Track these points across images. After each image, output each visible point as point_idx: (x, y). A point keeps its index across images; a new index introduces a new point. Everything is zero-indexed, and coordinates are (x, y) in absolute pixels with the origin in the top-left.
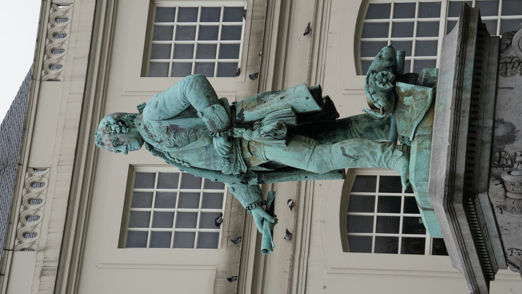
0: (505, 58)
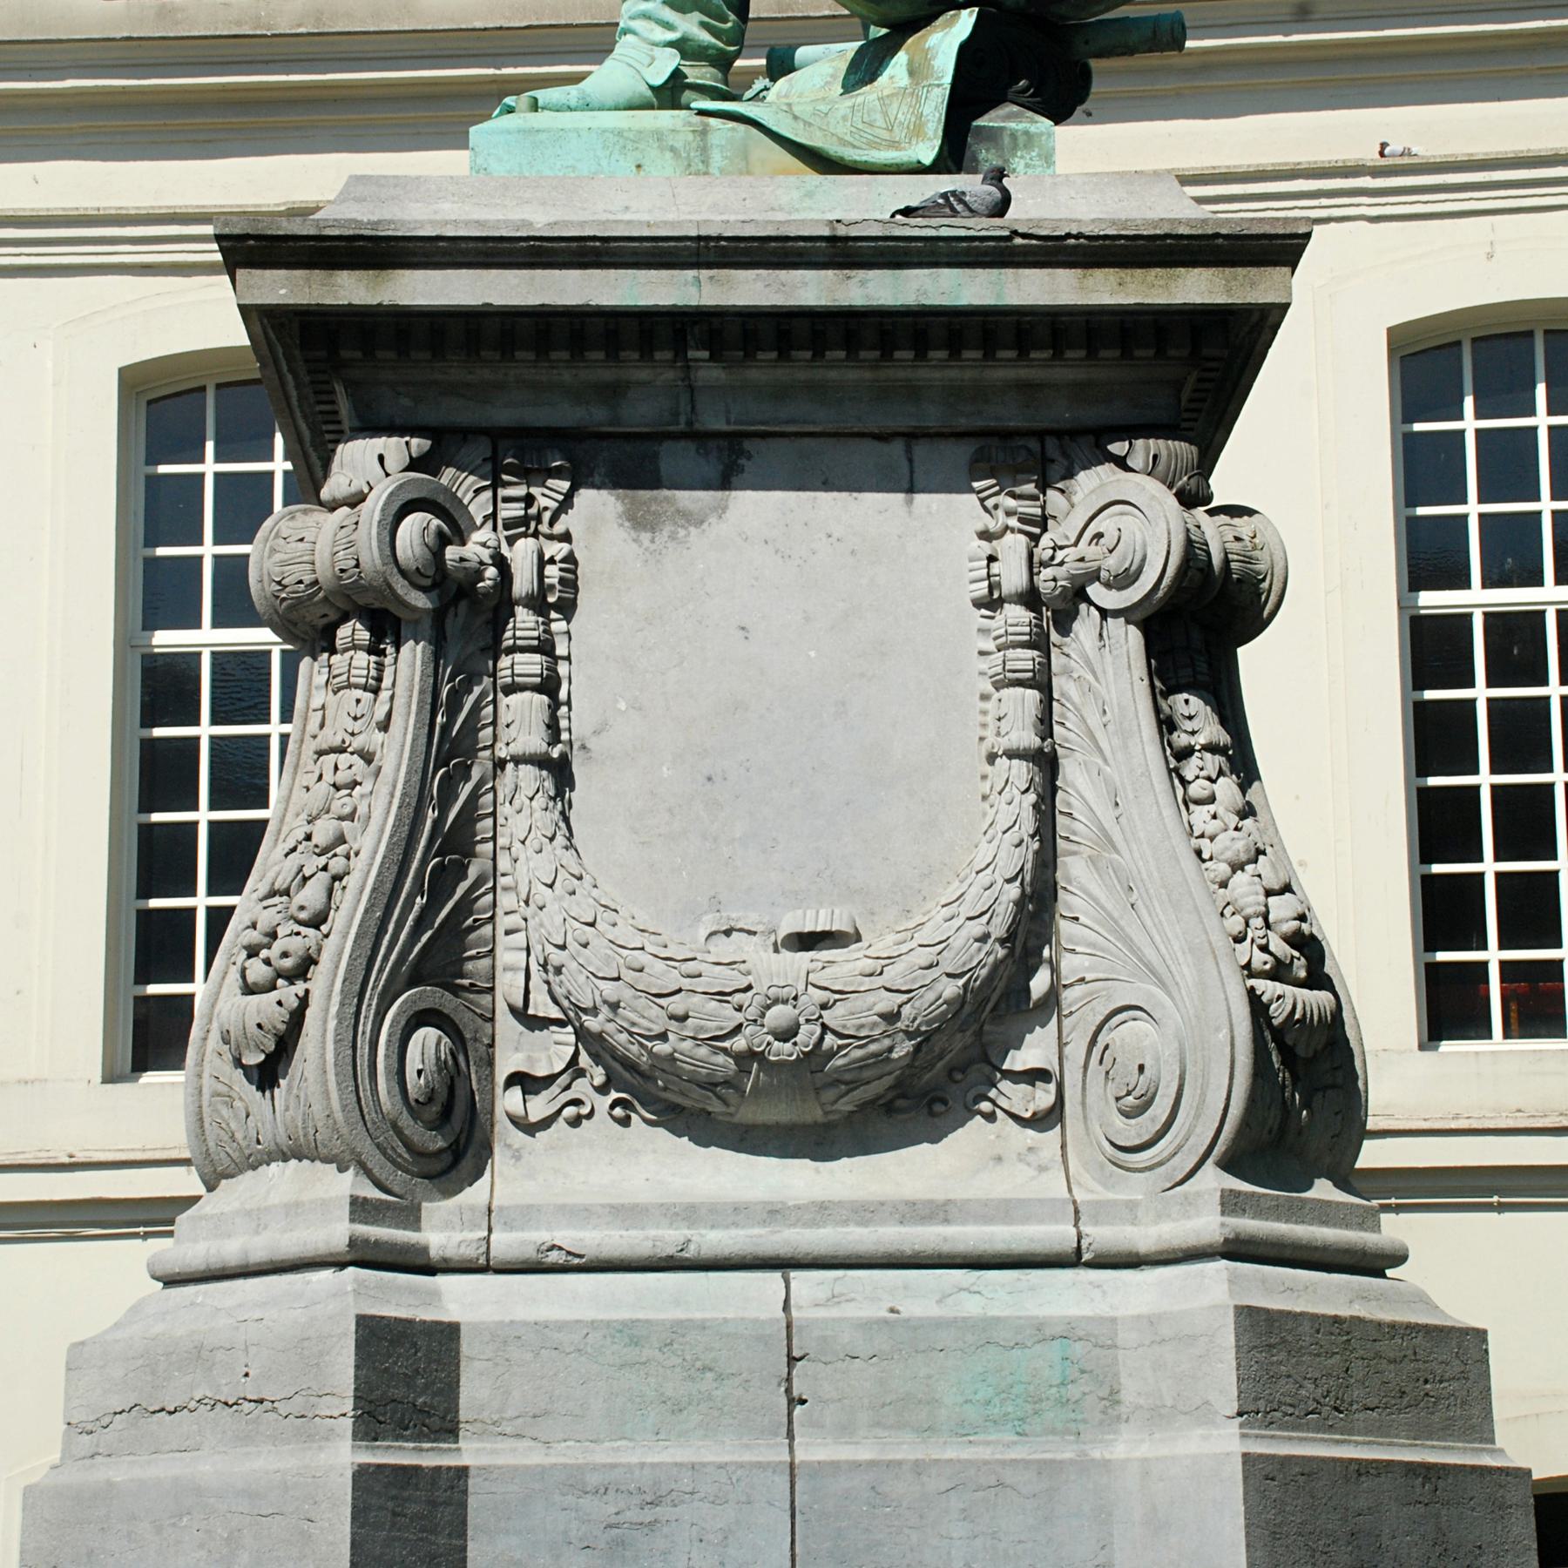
0: (1065, 454)
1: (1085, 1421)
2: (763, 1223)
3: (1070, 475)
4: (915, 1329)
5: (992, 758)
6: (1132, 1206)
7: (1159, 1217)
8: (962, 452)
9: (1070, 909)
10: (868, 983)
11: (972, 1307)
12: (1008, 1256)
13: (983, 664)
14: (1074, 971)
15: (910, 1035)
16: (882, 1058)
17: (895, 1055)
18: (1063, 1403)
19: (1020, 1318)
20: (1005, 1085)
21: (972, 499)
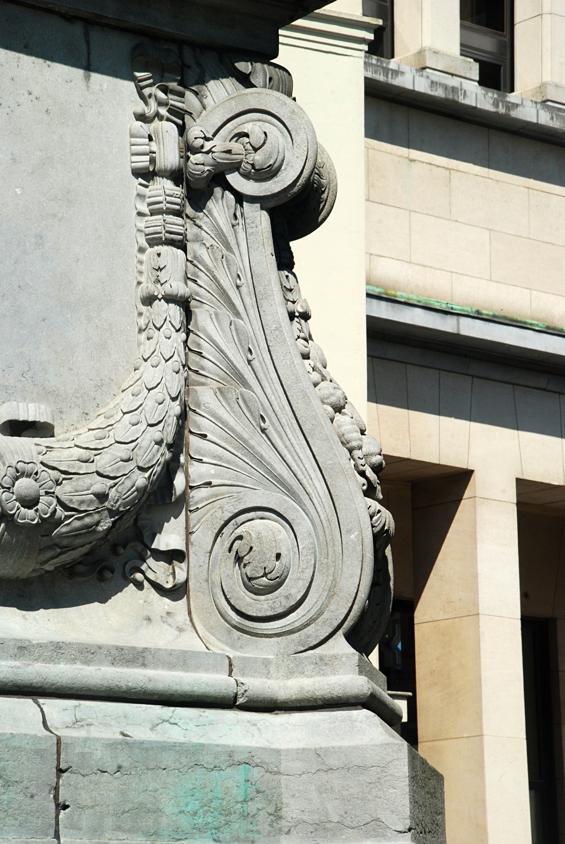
1: (258, 832)
2: (15, 657)
3: (202, 81)
4: (147, 750)
5: (149, 300)
6: (266, 663)
7: (291, 673)
8: (123, 44)
9: (199, 427)
10: (84, 468)
11: (175, 735)
12: (191, 696)
13: (142, 223)
14: (201, 477)
15: (111, 513)
16: (90, 529)
17: (100, 528)
18: (245, 816)
19: (218, 746)
20: (151, 561)
21: (130, 86)
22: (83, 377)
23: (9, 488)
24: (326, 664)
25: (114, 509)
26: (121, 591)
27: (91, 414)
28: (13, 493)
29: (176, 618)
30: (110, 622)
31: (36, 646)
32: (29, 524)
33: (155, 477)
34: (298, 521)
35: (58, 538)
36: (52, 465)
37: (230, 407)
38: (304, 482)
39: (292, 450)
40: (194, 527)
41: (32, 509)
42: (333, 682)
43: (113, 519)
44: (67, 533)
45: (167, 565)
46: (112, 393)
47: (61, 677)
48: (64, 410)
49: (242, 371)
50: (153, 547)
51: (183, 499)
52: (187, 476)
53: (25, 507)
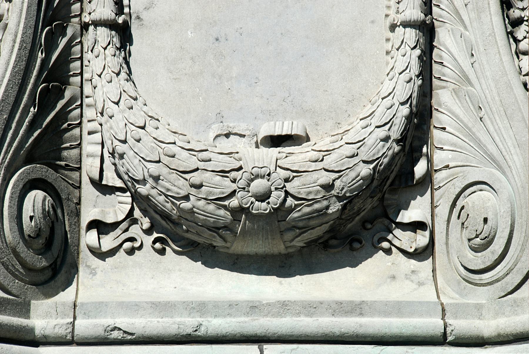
2: (247, 314)
5: (393, 27)
6: (479, 307)
7: (497, 315)
9: (440, 122)
12: (400, 337)
14: (442, 161)
15: (339, 199)
16: (322, 213)
17: (330, 211)
20: (398, 232)
22: (336, 95)
23: (244, 188)
24: (518, 306)
25: (340, 195)
26: (371, 257)
27: (343, 123)
28: (249, 191)
29: (419, 275)
30: (356, 282)
31: (265, 305)
32: (262, 213)
33: (382, 167)
34: (501, 190)
35: (293, 222)
36: (285, 167)
37: (461, 103)
38: (507, 157)
39: (499, 133)
40: (437, 202)
41: (264, 202)
42: (518, 320)
43: (341, 203)
44: (299, 217)
45: (413, 233)
46: (362, 105)
47: (281, 328)
48: (319, 122)
49: (467, 74)
50: (397, 221)
51: (427, 179)
52: (430, 161)
53: (259, 201)
